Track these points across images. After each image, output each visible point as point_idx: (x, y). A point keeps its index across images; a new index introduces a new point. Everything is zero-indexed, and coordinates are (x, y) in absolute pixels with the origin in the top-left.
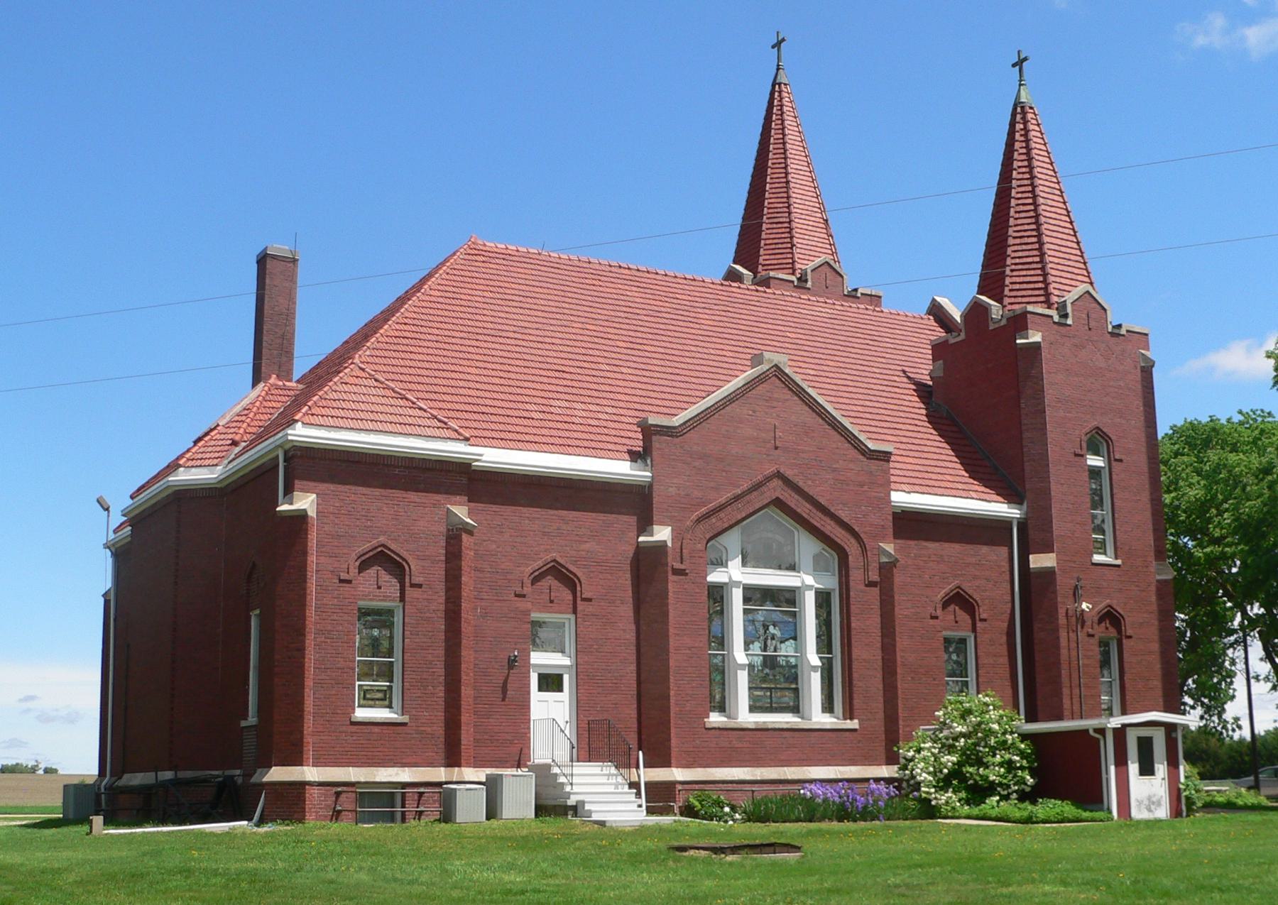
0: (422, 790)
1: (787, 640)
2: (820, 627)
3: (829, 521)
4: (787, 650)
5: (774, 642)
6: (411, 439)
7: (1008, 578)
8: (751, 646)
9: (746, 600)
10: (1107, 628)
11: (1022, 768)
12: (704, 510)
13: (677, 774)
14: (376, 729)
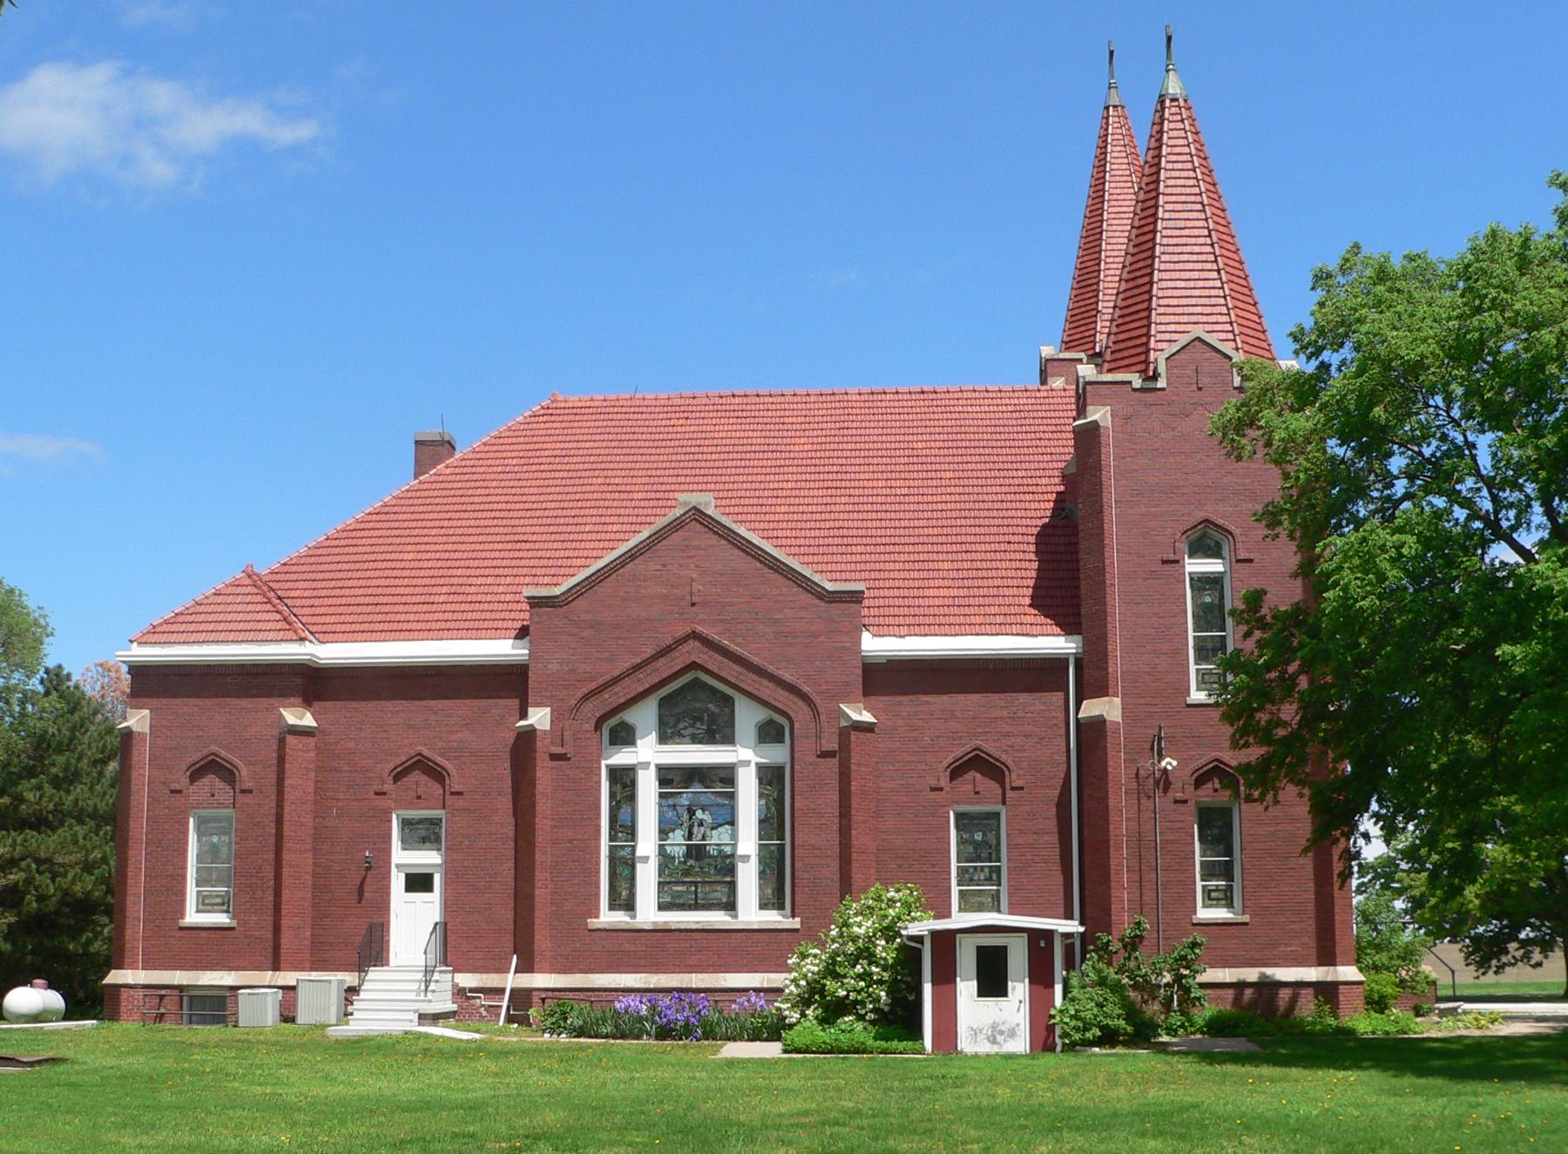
0: (163, 992)
1: (720, 825)
2: (768, 808)
3: (765, 682)
4: (719, 837)
5: (702, 829)
6: (244, 646)
7: (1063, 731)
8: (671, 835)
9: (663, 782)
10: (1216, 790)
11: (880, 982)
12: (593, 685)
13: (541, 980)
14: (204, 934)
